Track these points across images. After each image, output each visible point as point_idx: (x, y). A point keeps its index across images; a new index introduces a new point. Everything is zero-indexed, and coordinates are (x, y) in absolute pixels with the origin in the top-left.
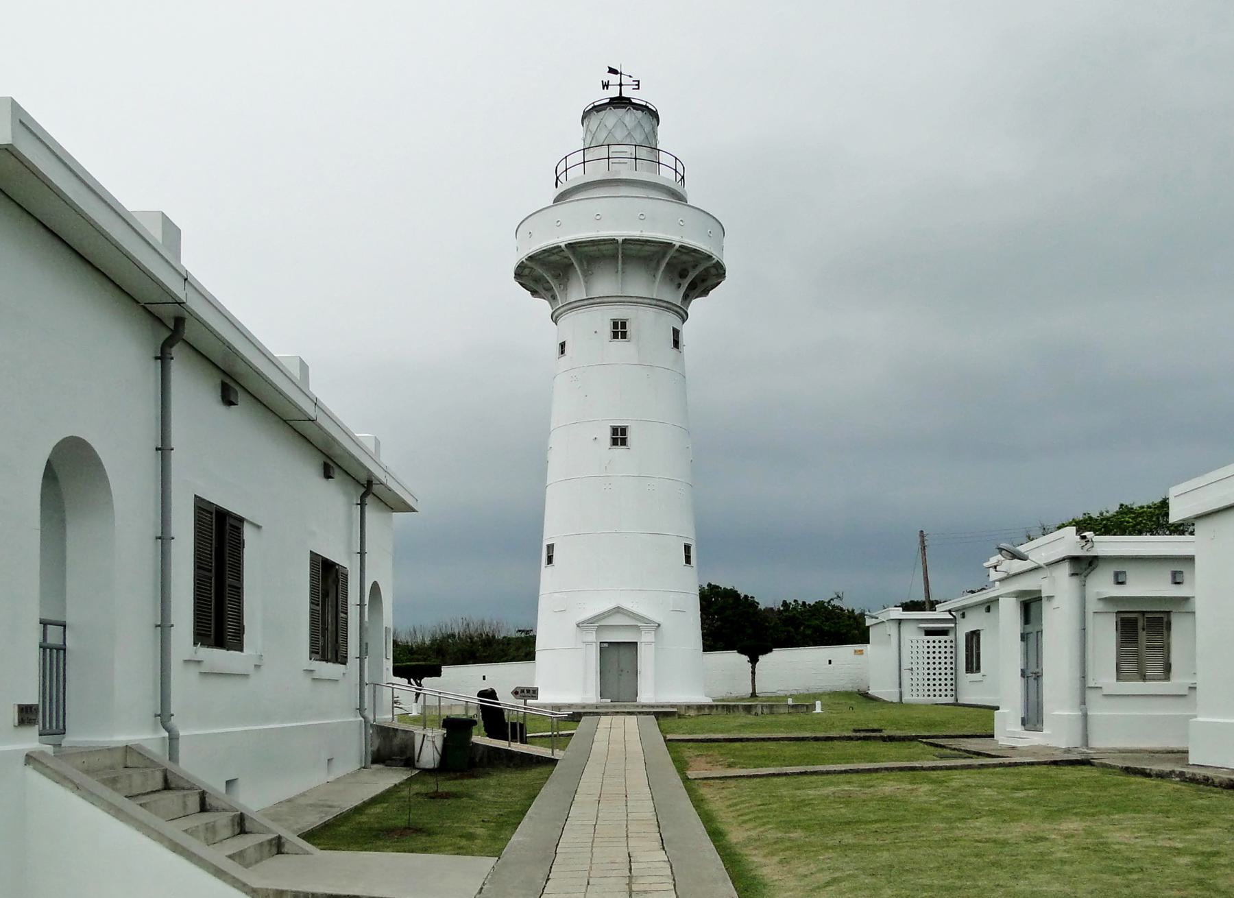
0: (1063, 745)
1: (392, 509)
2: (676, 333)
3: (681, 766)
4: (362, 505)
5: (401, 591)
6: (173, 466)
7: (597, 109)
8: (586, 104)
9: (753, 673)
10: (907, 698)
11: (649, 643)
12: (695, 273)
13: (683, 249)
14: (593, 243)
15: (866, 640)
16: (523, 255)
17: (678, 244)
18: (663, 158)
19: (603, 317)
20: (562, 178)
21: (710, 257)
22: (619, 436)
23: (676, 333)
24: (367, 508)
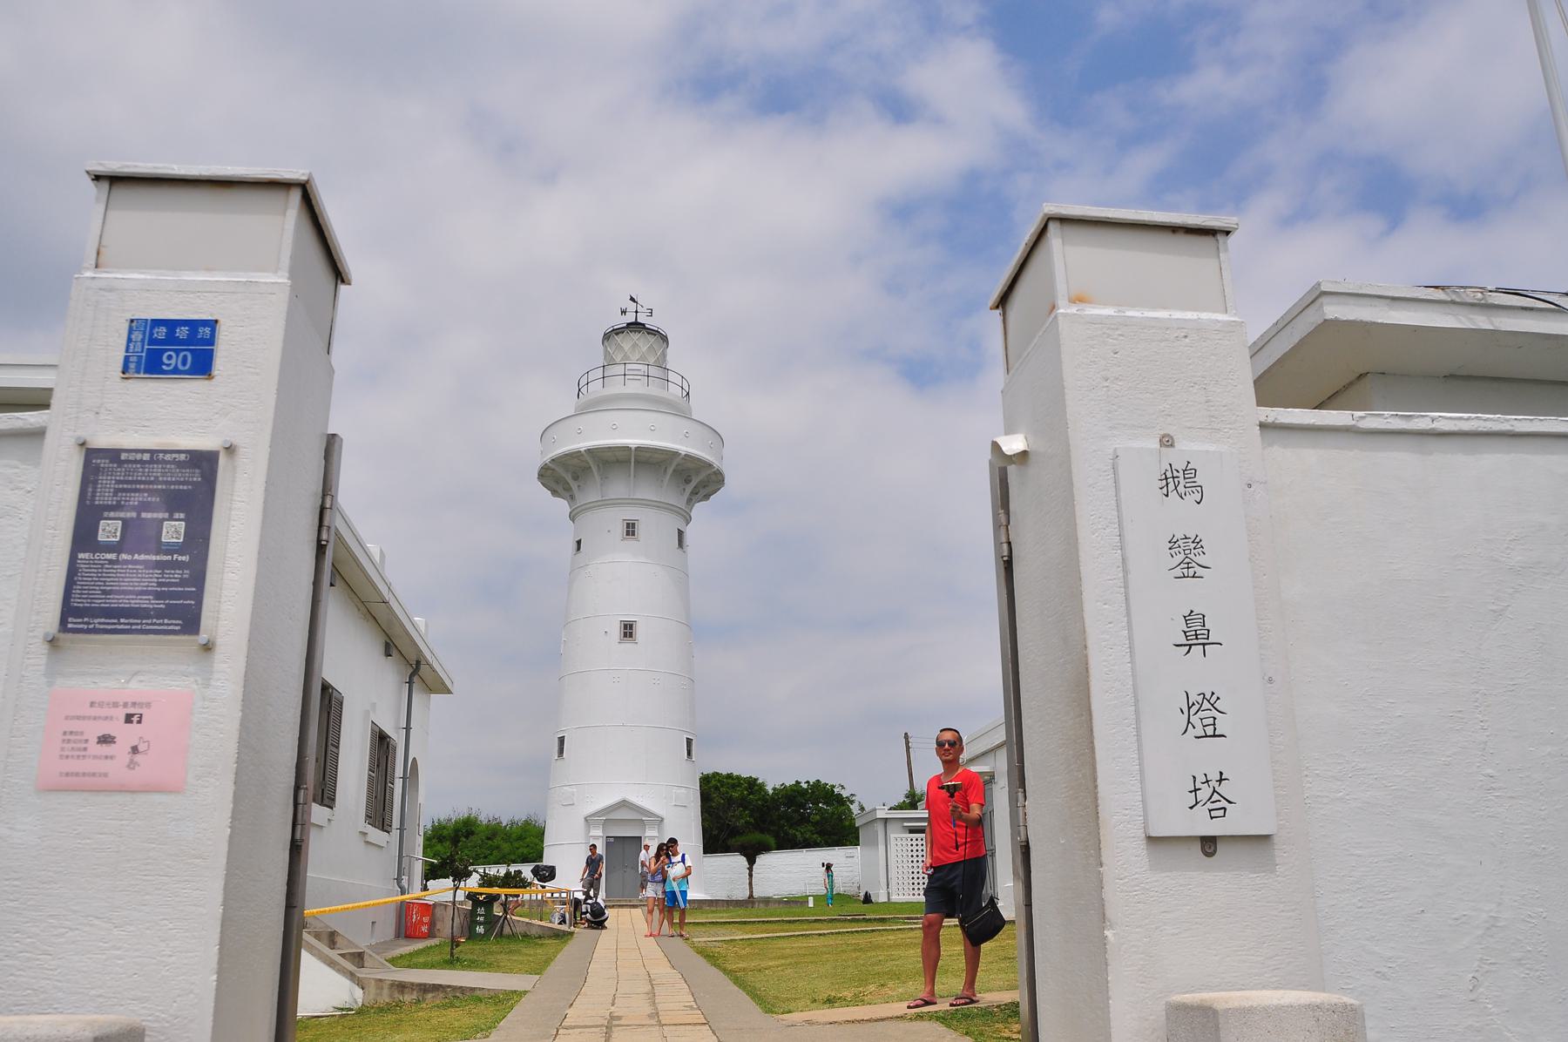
0: (1276, 448)
2: (680, 533)
4: (410, 683)
5: (443, 792)
7: (617, 331)
8: (606, 327)
9: (751, 875)
10: (894, 898)
12: (696, 479)
14: (610, 449)
16: (547, 458)
18: (672, 376)
21: (710, 465)
22: (628, 630)
23: (680, 533)
24: (415, 686)
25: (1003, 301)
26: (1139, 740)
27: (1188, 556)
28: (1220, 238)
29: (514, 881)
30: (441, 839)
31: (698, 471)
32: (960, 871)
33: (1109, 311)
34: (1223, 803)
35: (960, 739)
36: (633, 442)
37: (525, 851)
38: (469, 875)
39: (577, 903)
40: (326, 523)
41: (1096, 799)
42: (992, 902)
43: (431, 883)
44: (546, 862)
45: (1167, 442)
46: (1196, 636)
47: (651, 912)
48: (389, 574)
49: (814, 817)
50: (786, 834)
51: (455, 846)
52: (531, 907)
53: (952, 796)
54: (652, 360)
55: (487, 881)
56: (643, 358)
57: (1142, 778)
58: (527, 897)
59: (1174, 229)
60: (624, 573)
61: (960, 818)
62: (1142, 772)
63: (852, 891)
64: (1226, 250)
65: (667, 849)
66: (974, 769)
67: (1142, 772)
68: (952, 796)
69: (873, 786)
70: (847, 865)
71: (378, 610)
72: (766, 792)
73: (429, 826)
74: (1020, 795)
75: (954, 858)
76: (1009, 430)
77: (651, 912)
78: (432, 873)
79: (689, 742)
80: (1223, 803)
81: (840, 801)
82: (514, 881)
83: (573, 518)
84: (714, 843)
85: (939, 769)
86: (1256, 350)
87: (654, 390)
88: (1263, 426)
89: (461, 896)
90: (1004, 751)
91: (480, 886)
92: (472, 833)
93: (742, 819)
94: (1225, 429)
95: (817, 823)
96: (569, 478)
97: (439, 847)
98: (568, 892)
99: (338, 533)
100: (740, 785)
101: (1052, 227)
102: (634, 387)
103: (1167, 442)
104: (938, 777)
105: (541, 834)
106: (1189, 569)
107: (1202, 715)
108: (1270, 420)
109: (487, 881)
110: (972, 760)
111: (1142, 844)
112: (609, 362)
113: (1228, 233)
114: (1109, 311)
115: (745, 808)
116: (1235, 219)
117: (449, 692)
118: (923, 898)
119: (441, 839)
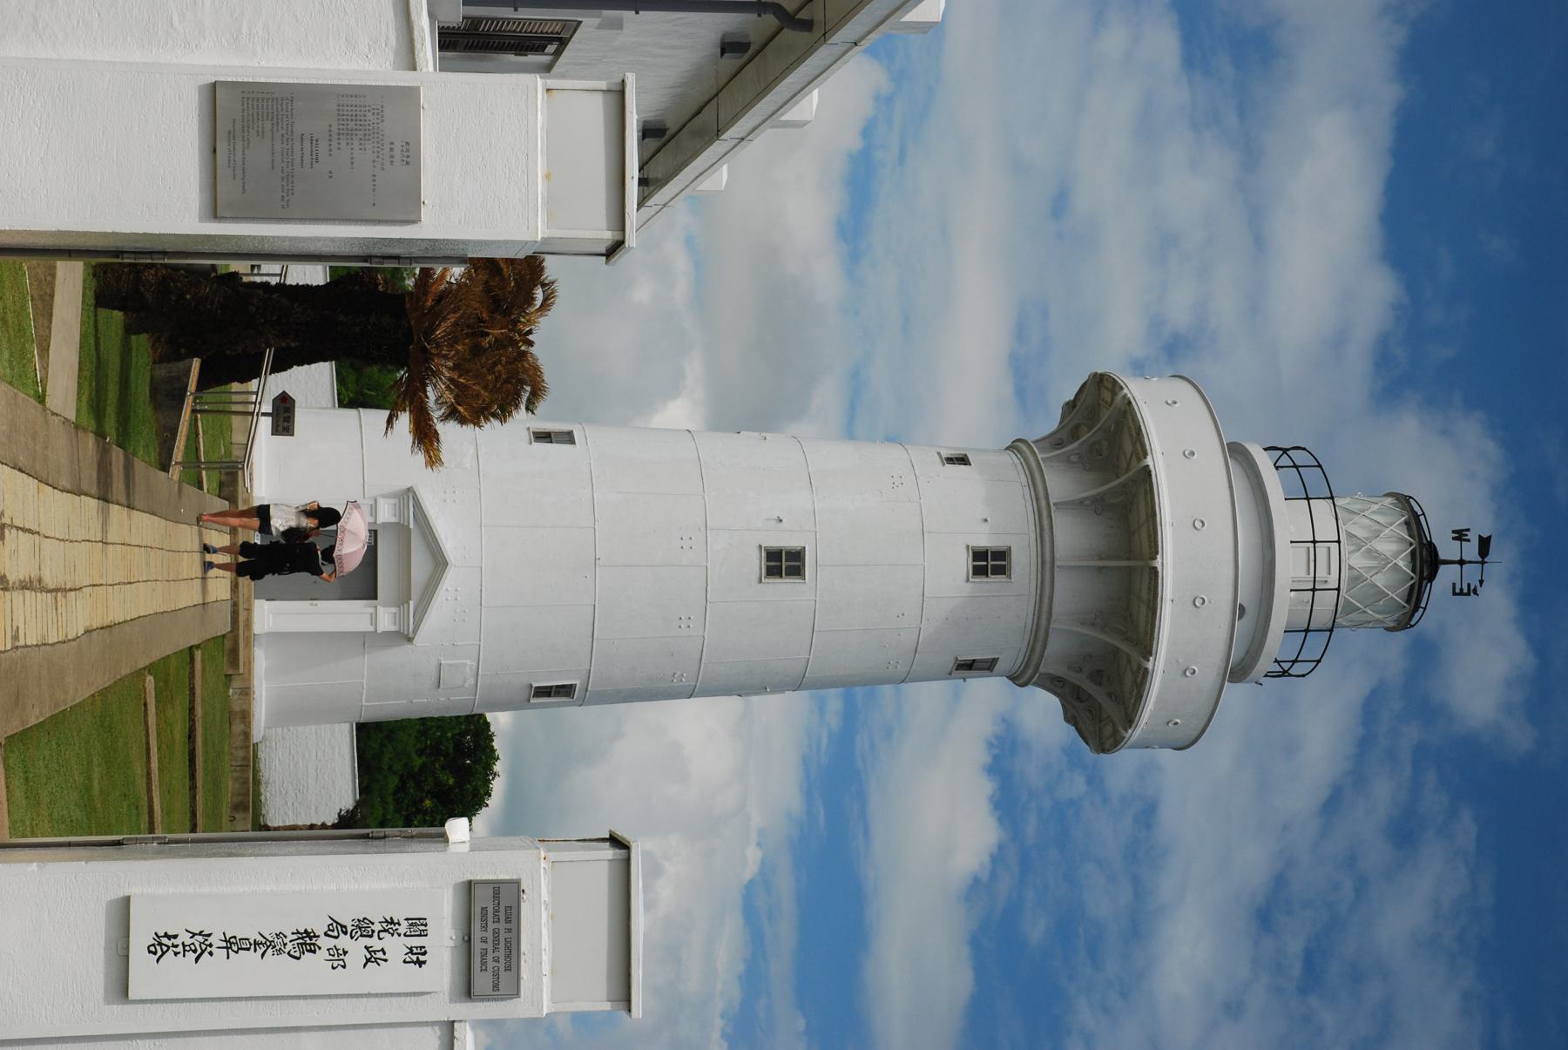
3: (150, 669)
6: (94, 865)
11: (374, 619)
13: (1142, 677)
14: (1152, 515)
17: (1150, 666)
31: (1116, 697)
36: (1169, 563)
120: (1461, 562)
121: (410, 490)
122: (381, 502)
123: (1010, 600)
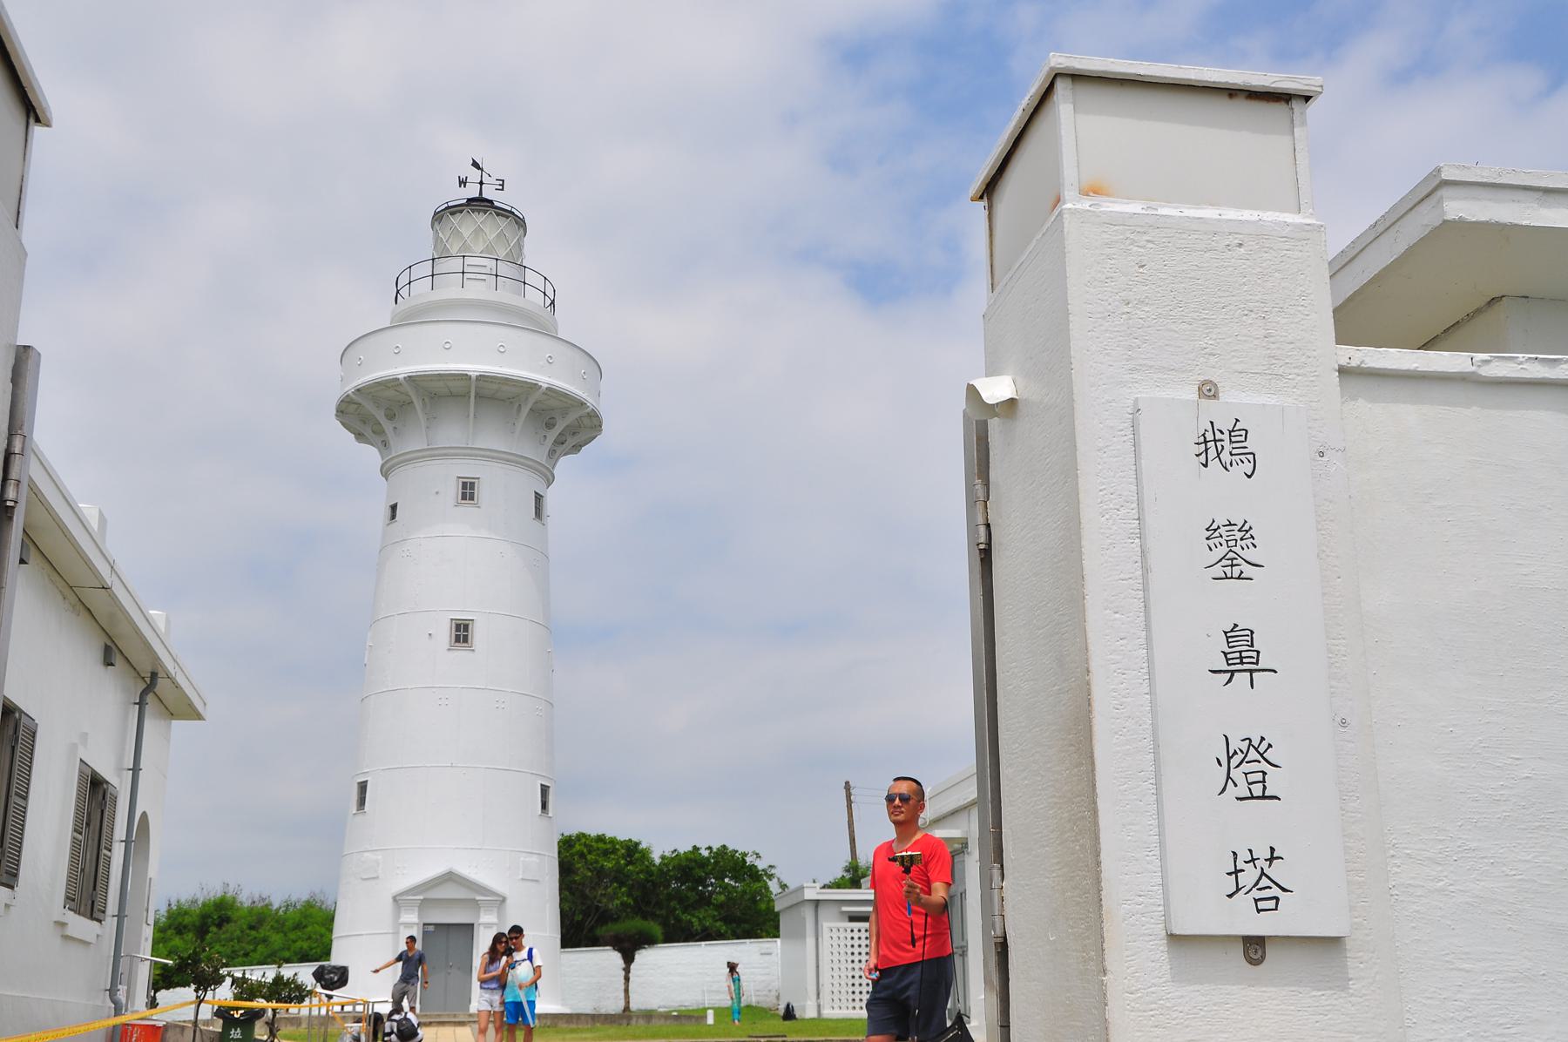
1: (172, 715)
2: (539, 498)
4: (141, 704)
5: (180, 866)
7: (453, 210)
8: (439, 202)
9: (627, 979)
10: (827, 1012)
12: (562, 423)
13: (551, 391)
14: (441, 377)
15: (775, 934)
16: (350, 387)
18: (530, 277)
19: (445, 475)
20: (404, 292)
21: (582, 404)
22: (462, 633)
23: (539, 498)
24: (148, 709)
25: (990, 189)
26: (1159, 802)
27: (1232, 547)
28: (1296, 105)
29: (285, 991)
30: (180, 930)
31: (565, 412)
32: (915, 976)
33: (1135, 207)
34: (1275, 891)
35: (920, 793)
36: (474, 368)
37: (305, 945)
38: (219, 980)
39: (378, 1019)
40: (14, 474)
41: (1098, 881)
42: (960, 1021)
43: (163, 996)
44: (336, 960)
45: (1208, 391)
46: (1241, 657)
47: (483, 1031)
48: (113, 547)
49: (713, 897)
50: (678, 920)
51: (200, 942)
52: (310, 1025)
53: (907, 871)
54: (502, 254)
55: (246, 990)
56: (489, 249)
57: (1163, 854)
58: (305, 1012)
59: (1232, 92)
60: (457, 549)
61: (918, 901)
62: (1162, 844)
63: (767, 1001)
64: (1304, 123)
65: (507, 943)
66: (939, 833)
67: (1162, 844)
68: (907, 871)
69: (802, 852)
70: (760, 964)
71: (96, 600)
72: (652, 863)
73: (163, 910)
74: (996, 873)
75: (908, 957)
76: (992, 370)
77: (483, 1031)
78: (164, 979)
79: (545, 790)
80: (1275, 891)
81: (754, 875)
82: (285, 991)
83: (386, 472)
84: (576, 933)
85: (890, 833)
86: (1340, 266)
87: (505, 295)
88: (1343, 371)
89: (206, 1012)
90: (975, 812)
91: (237, 997)
92: (228, 920)
93: (617, 897)
94: (1291, 382)
95: (720, 906)
96: (380, 416)
97: (177, 942)
98: (366, 1003)
99: (32, 487)
100: (614, 851)
101: (1060, 86)
102: (477, 290)
103: (1208, 391)
104: (888, 846)
105: (328, 920)
106: (1233, 568)
107: (1248, 767)
108: (1354, 363)
109: (246, 990)
110: (938, 821)
111: (1162, 944)
112: (440, 255)
113: (1307, 99)
114: (1135, 207)
115: (622, 884)
116: (1318, 80)
117: (199, 717)
118: (864, 1014)
119: (180, 930)
120: (481, 183)
121: (395, 899)
122: (402, 920)
123: (491, 477)
